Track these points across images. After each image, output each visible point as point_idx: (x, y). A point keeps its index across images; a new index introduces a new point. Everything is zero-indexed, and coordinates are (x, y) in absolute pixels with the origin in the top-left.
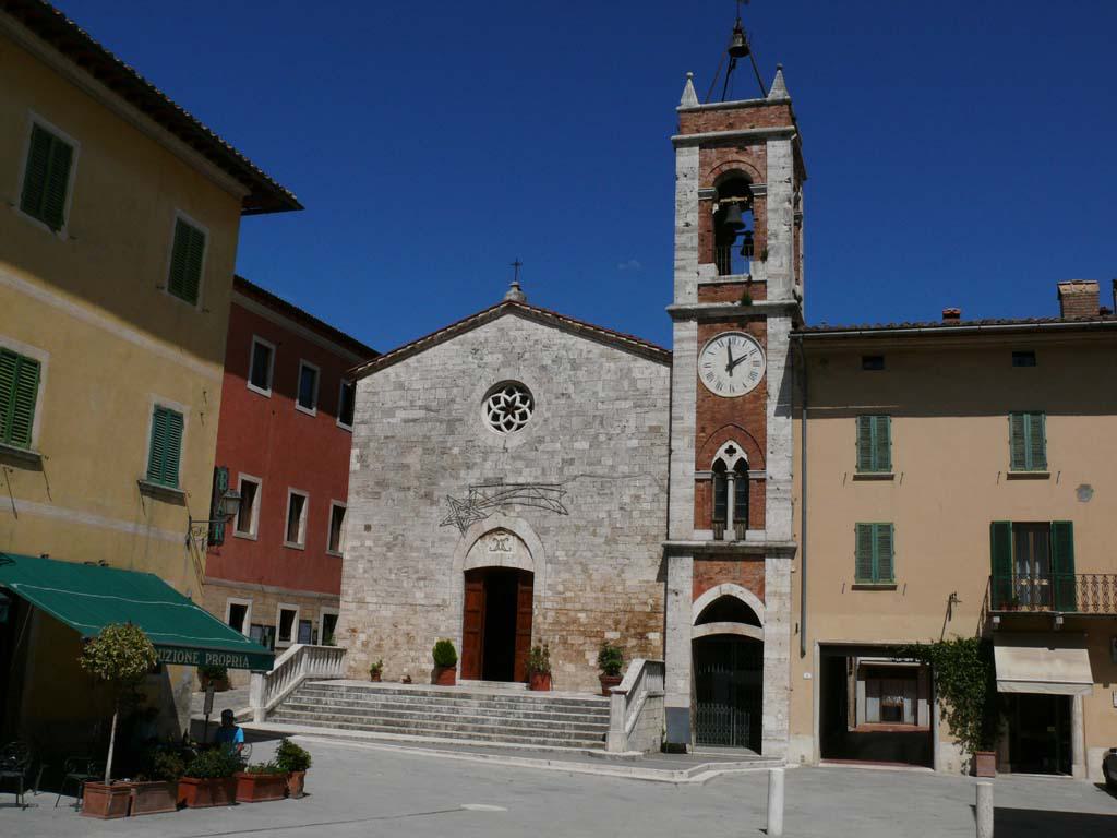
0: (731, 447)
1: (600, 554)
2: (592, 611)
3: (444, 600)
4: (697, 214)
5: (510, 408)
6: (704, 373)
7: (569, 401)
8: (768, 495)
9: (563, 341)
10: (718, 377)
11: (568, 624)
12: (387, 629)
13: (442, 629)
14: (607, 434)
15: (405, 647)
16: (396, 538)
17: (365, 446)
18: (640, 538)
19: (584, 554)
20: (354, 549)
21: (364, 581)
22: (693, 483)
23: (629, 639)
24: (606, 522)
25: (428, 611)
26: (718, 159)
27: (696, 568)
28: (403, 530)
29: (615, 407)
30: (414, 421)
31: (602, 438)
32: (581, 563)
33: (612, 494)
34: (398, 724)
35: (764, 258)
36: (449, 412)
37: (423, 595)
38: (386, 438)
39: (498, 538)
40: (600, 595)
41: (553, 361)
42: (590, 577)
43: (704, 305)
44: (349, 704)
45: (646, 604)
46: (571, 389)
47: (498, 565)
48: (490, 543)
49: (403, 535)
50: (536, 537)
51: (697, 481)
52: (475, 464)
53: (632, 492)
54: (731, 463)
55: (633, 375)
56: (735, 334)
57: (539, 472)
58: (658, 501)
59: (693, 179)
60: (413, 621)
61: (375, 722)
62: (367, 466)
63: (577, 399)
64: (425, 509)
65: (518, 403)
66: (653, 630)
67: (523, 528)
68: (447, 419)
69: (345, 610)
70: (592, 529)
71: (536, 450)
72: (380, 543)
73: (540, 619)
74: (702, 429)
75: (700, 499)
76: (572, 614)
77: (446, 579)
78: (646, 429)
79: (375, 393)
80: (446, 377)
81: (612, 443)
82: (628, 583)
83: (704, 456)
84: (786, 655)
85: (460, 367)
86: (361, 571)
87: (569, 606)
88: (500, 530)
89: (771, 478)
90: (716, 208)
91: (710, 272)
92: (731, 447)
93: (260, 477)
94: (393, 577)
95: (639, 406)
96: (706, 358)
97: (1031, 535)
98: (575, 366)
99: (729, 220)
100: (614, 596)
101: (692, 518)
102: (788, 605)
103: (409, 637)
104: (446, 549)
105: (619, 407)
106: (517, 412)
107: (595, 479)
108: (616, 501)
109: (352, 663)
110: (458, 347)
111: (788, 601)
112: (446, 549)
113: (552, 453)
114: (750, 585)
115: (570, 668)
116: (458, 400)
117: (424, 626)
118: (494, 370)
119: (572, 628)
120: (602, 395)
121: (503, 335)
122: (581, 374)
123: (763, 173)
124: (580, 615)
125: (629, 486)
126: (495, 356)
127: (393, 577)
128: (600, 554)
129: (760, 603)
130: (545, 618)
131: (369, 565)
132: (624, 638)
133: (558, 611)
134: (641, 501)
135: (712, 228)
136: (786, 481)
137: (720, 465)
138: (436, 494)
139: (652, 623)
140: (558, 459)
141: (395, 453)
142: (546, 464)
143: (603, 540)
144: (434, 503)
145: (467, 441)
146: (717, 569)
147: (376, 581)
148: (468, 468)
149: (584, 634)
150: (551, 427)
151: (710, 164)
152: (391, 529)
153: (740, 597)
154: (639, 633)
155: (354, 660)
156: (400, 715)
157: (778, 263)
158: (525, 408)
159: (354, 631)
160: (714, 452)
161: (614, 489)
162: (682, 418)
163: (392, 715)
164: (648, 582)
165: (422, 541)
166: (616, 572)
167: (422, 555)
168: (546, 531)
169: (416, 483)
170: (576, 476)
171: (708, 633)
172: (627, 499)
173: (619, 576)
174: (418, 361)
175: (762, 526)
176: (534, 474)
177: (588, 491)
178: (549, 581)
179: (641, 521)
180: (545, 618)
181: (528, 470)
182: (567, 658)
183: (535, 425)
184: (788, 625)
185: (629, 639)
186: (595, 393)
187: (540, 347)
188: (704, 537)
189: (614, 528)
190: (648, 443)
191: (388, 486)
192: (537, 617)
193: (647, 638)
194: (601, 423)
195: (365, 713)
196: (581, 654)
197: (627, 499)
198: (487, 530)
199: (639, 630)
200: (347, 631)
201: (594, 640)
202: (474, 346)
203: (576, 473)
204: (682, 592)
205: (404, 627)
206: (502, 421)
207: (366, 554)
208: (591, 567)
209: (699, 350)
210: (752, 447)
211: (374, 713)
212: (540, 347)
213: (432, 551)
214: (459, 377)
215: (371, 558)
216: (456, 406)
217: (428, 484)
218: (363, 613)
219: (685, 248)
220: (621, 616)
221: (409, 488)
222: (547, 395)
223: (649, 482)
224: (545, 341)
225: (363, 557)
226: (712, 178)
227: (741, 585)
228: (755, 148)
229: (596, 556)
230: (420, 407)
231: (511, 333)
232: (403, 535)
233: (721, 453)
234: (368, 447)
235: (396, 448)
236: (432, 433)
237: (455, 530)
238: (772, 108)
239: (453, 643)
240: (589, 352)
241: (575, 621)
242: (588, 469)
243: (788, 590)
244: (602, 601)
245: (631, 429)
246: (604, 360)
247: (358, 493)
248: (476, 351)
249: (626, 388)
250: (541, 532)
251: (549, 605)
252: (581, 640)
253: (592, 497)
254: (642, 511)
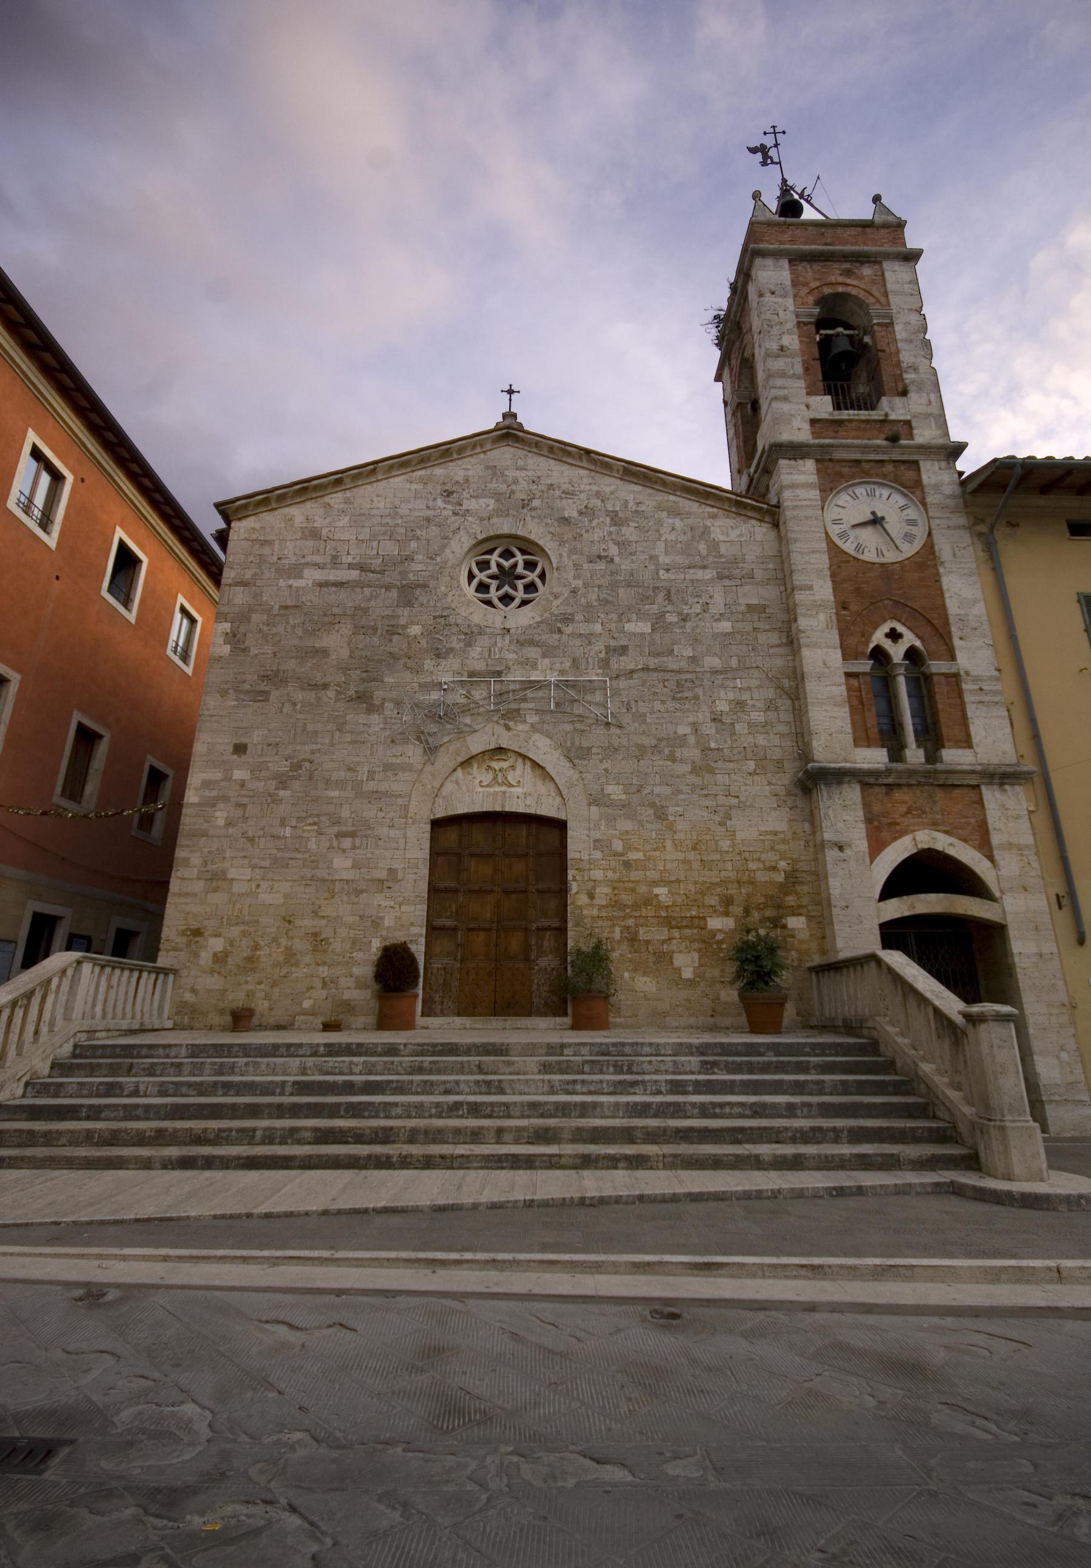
0: (893, 630)
1: (686, 789)
2: (678, 881)
5: (507, 576)
7: (612, 567)
8: (968, 698)
9: (595, 488)
11: (636, 906)
13: (388, 922)
14: (679, 614)
15: (308, 958)
18: (751, 765)
19: (657, 790)
20: (207, 784)
22: (843, 679)
24: (692, 740)
26: (816, 279)
28: (313, 752)
29: (688, 577)
31: (671, 618)
32: (652, 805)
33: (696, 698)
34: (359, 1138)
35: (904, 393)
36: (404, 574)
37: (348, 863)
38: (282, 607)
39: (496, 765)
40: (692, 856)
41: (581, 513)
42: (671, 827)
43: (817, 441)
44: (201, 1089)
45: (774, 869)
46: (614, 550)
47: (498, 809)
48: (480, 775)
50: (568, 764)
51: (848, 675)
53: (731, 696)
54: (897, 652)
56: (875, 483)
57: (568, 664)
58: (777, 709)
59: (785, 296)
61: (291, 1136)
62: (245, 650)
64: (356, 718)
67: (543, 749)
69: (180, 895)
70: (667, 751)
71: (560, 631)
73: (583, 899)
74: (842, 606)
75: (856, 702)
76: (643, 889)
77: (393, 833)
78: (743, 608)
79: (265, 543)
80: (397, 525)
81: (689, 624)
82: (740, 835)
83: (852, 641)
84: (1049, 947)
85: (421, 514)
86: (221, 822)
87: (635, 875)
89: (967, 673)
91: (823, 406)
92: (893, 630)
93: (19, 672)
94: (288, 832)
95: (729, 578)
98: (616, 520)
100: (717, 857)
101: (848, 729)
102: (1036, 865)
103: (318, 942)
104: (400, 784)
105: (694, 577)
107: (668, 676)
108: (704, 708)
109: (188, 997)
110: (420, 486)
111: (1033, 858)
112: (400, 784)
113: (589, 638)
115: (645, 984)
117: (350, 919)
118: (482, 519)
119: (644, 912)
120: (663, 559)
121: (494, 474)
122: (629, 532)
123: (883, 300)
124: (657, 891)
125: (722, 686)
126: (482, 501)
128: (686, 789)
129: (987, 864)
130: (591, 896)
133: (614, 885)
135: (817, 356)
137: (879, 655)
138: (379, 694)
139: (790, 900)
140: (599, 646)
143: (687, 768)
144: (371, 709)
146: (903, 809)
147: (251, 840)
148: (438, 656)
149: (668, 922)
150: (583, 601)
151: (806, 284)
152: (289, 752)
153: (951, 852)
154: (769, 919)
155: (193, 991)
156: (355, 1111)
157: (924, 401)
158: (520, 595)
159: (198, 932)
160: (867, 636)
161: (699, 691)
163: (333, 1111)
164: (776, 833)
165: (350, 769)
166: (717, 818)
168: (585, 753)
170: (632, 672)
171: (906, 914)
172: (723, 706)
173: (722, 824)
175: (967, 742)
176: (558, 666)
177: (655, 694)
178: (596, 835)
180: (591, 896)
181: (546, 660)
182: (638, 967)
183: (556, 597)
184: (1043, 897)
186: (653, 558)
187: (557, 493)
188: (875, 758)
189: (706, 750)
191: (284, 682)
193: (784, 927)
194: (668, 597)
195: (254, 1111)
196: (663, 958)
199: (769, 913)
201: (687, 932)
203: (632, 666)
205: (306, 923)
206: (494, 594)
208: (671, 810)
211: (281, 1111)
213: (371, 786)
215: (245, 800)
216: (415, 567)
217: (363, 680)
221: (325, 686)
223: (757, 683)
225: (225, 799)
226: (811, 299)
227: (946, 832)
228: (867, 271)
229: (679, 792)
230: (351, 566)
231: (507, 473)
233: (879, 637)
234: (249, 621)
236: (373, 603)
237: (413, 753)
238: (883, 231)
239: (413, 948)
241: (649, 900)
242: (653, 662)
243: (1030, 840)
244: (696, 865)
246: (664, 514)
248: (449, 493)
249: (704, 553)
250: (575, 755)
252: (664, 934)
253: (663, 702)
254: (750, 725)
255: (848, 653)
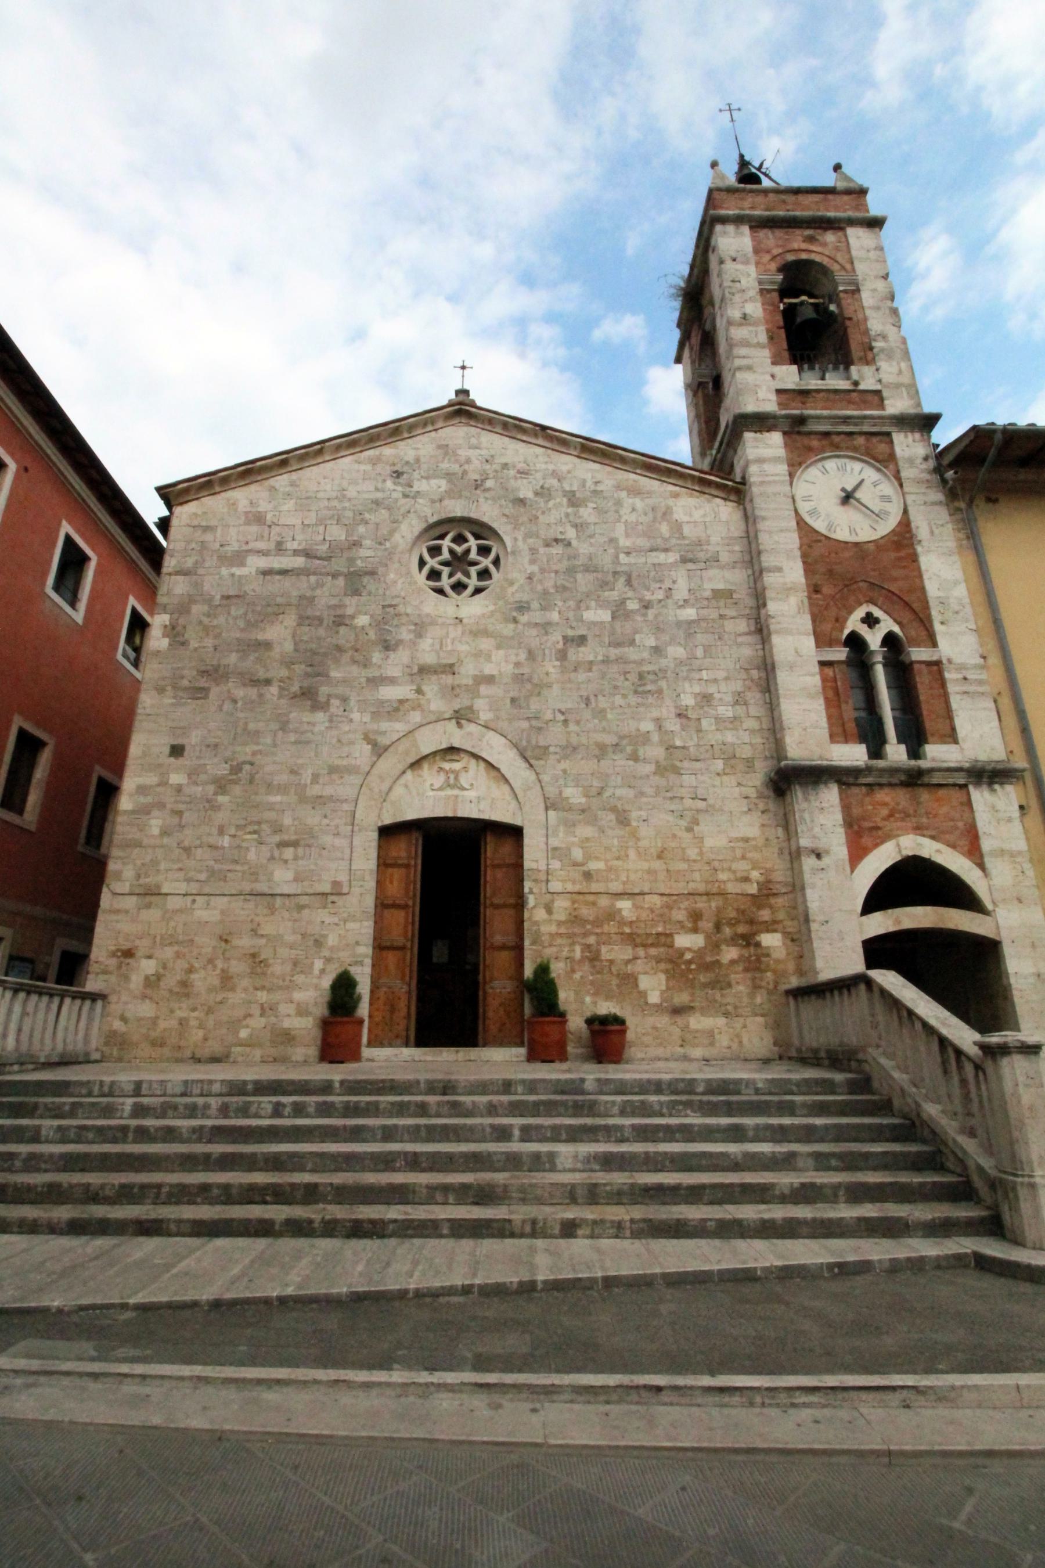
3: (336, 884)
4: (759, 305)
6: (804, 508)
7: (569, 550)
9: (551, 467)
10: (828, 515)
12: (207, 943)
13: (332, 940)
14: (641, 600)
16: (237, 769)
17: (183, 608)
20: (142, 790)
21: (159, 852)
22: (816, 669)
23: (724, 947)
24: (655, 737)
25: (301, 908)
27: (846, 808)
28: (254, 754)
29: (650, 561)
30: (284, 572)
32: (614, 809)
33: (660, 692)
36: (351, 560)
37: (290, 875)
39: (447, 766)
40: (658, 865)
41: (537, 494)
42: (634, 835)
45: (746, 879)
46: (571, 533)
47: (450, 814)
48: (430, 777)
49: (252, 764)
50: (524, 765)
51: (823, 664)
52: (399, 642)
53: (697, 689)
54: (874, 639)
55: (675, 516)
57: (523, 656)
60: (267, 929)
63: (583, 549)
65: (473, 555)
66: (770, 927)
68: (345, 570)
70: (629, 749)
72: (203, 777)
73: (540, 914)
74: (815, 589)
77: (341, 842)
79: (207, 529)
81: (651, 613)
82: (709, 843)
83: (827, 627)
86: (156, 831)
87: (595, 887)
88: (452, 751)
89: (950, 661)
90: (782, 307)
95: (691, 561)
96: (801, 488)
97: (542, 1108)
98: (573, 500)
99: (799, 320)
103: (256, 962)
105: (656, 561)
106: (459, 576)
108: (668, 702)
110: (368, 467)
111: (1027, 866)
113: (546, 627)
114: (951, 838)
116: (367, 542)
117: (290, 938)
118: (433, 501)
119: (606, 928)
121: (446, 454)
122: (587, 513)
123: (848, 266)
126: (434, 482)
127: (226, 841)
128: (650, 791)
129: (977, 872)
131: (176, 820)
132: (715, 946)
134: (715, 703)
136: (976, 667)
137: (855, 642)
138: (324, 690)
140: (556, 637)
141: (241, 624)
142: (535, 643)
143: (649, 768)
145: (384, 607)
148: (387, 648)
149: (631, 939)
150: (539, 588)
152: (228, 754)
153: (939, 859)
154: (743, 936)
155: (124, 1019)
157: (894, 369)
159: (129, 954)
160: (840, 621)
161: (663, 684)
162: (779, 569)
164: (746, 840)
165: (293, 772)
166: (683, 823)
167: (292, 798)
169: (284, 673)
172: (688, 700)
173: (689, 830)
174: (293, 484)
175: (951, 736)
176: (513, 658)
179: (719, 736)
180: (549, 910)
181: (502, 652)
185: (724, 947)
187: (512, 472)
189: (670, 748)
190: (714, 615)
192: (535, 913)
193: (758, 945)
194: (629, 582)
197: (688, 700)
198: (426, 750)
199: (741, 929)
200: (113, 954)
201: (653, 951)
202: (395, 468)
204: (827, 852)
205: (244, 942)
207: (169, 799)
208: (634, 815)
209: (791, 475)
210: (907, 617)
212: (512, 472)
213: (315, 790)
214: (370, 511)
216: (363, 553)
218: (153, 915)
219: (746, 343)
220: (701, 904)
221: (268, 682)
222: (531, 541)
224: (521, 466)
225: (161, 806)
227: (933, 838)
229: (642, 794)
230: (296, 553)
231: (460, 452)
232: (252, 764)
234: (188, 611)
235: (246, 614)
240: (597, 483)
241: (612, 915)
244: (662, 876)
245: (681, 591)
246: (624, 494)
247: (161, 690)
248: (398, 474)
251: (556, 886)
252: (627, 953)
253: (624, 696)
254: (718, 719)
255: (822, 640)
